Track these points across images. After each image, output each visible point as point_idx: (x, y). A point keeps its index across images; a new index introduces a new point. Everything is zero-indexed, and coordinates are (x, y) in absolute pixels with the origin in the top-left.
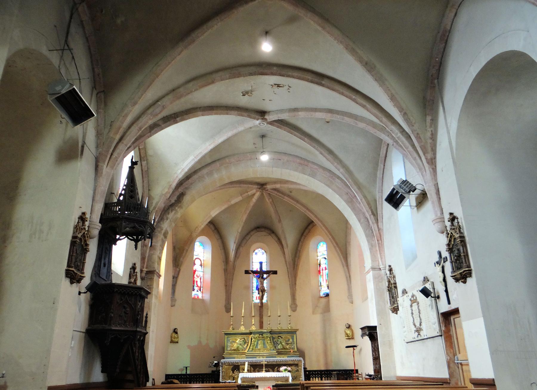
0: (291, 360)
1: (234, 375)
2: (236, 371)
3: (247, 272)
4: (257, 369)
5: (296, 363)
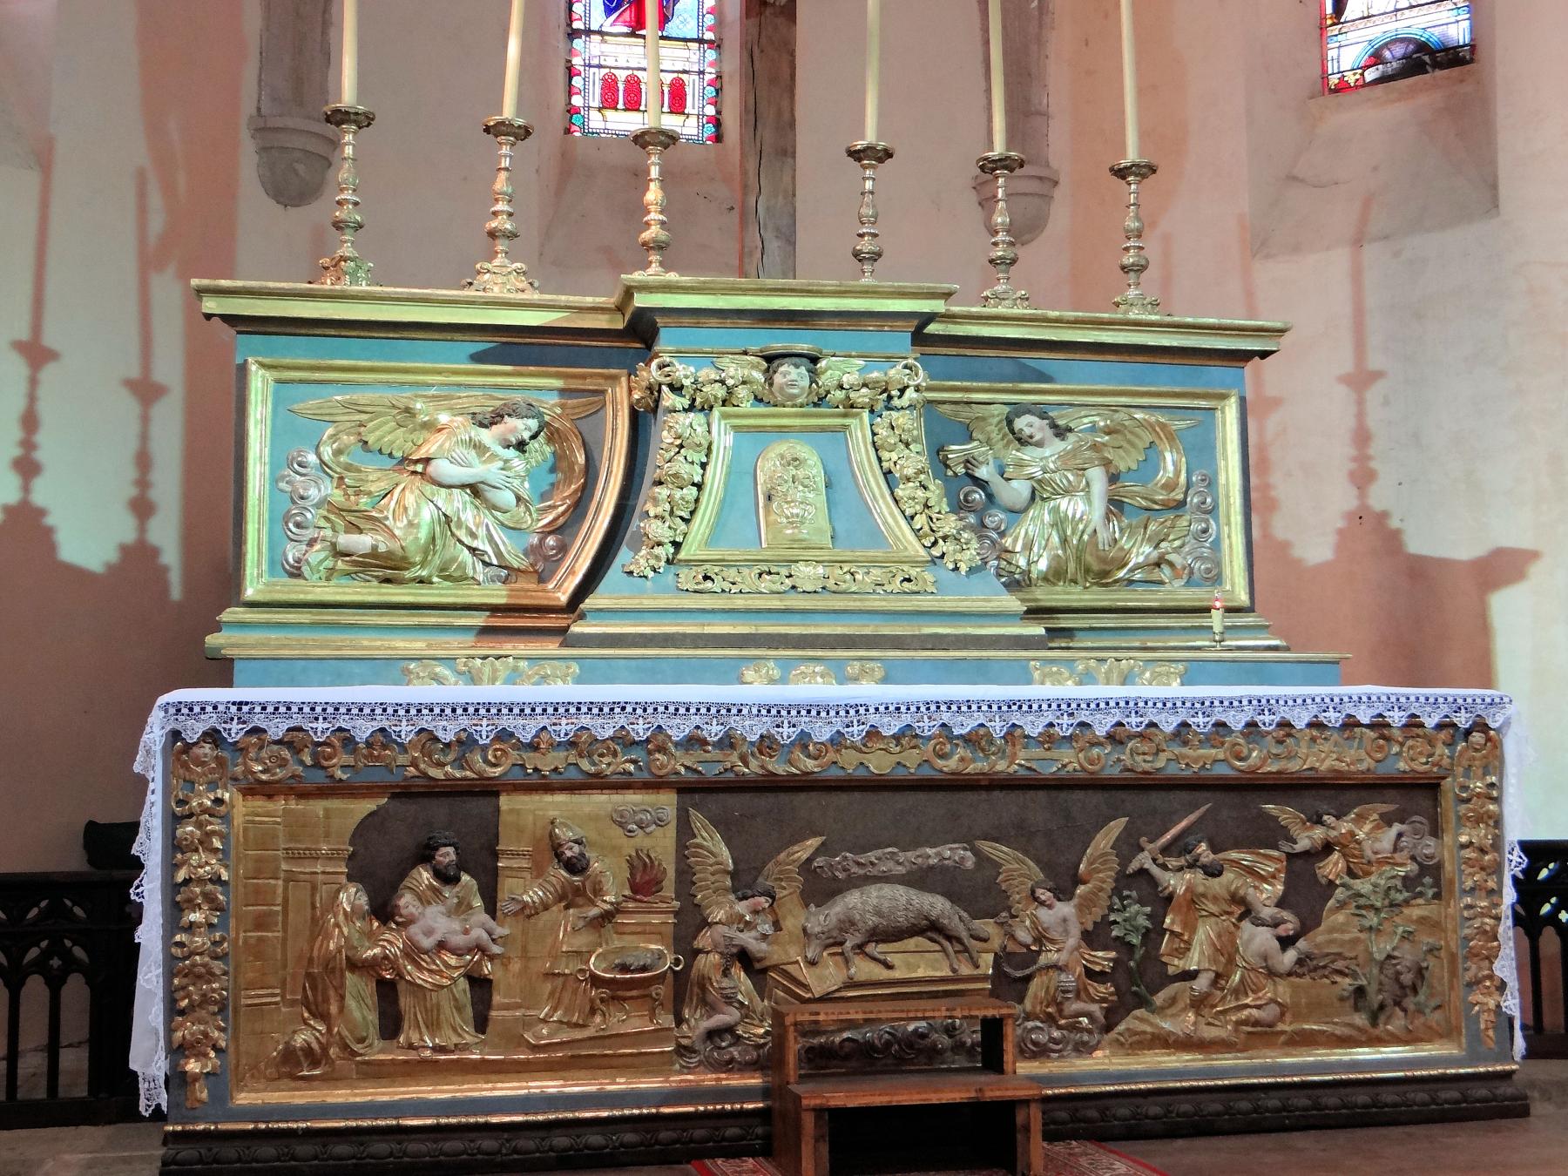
0: (1351, 724)
1: (392, 943)
2: (425, 876)
3: (525, 133)
4: (804, 849)
5: (1405, 761)
